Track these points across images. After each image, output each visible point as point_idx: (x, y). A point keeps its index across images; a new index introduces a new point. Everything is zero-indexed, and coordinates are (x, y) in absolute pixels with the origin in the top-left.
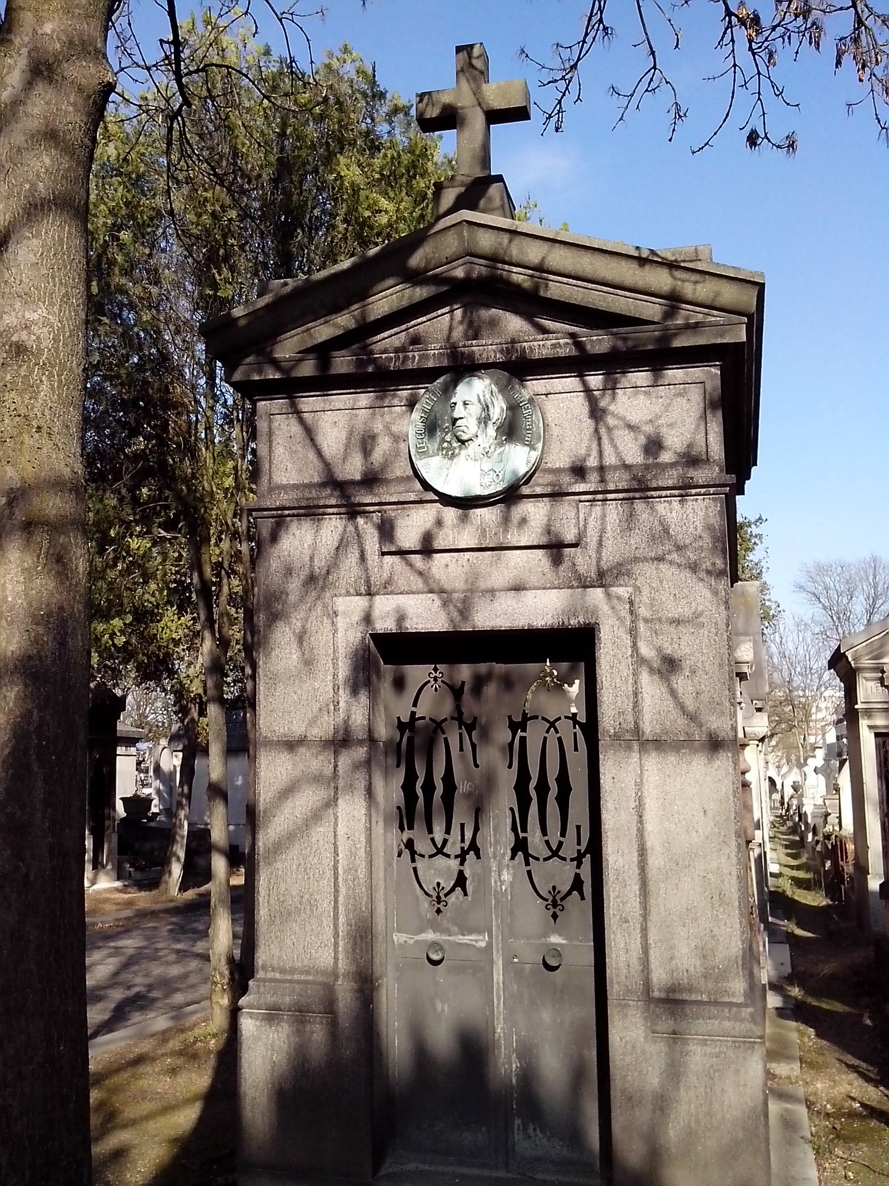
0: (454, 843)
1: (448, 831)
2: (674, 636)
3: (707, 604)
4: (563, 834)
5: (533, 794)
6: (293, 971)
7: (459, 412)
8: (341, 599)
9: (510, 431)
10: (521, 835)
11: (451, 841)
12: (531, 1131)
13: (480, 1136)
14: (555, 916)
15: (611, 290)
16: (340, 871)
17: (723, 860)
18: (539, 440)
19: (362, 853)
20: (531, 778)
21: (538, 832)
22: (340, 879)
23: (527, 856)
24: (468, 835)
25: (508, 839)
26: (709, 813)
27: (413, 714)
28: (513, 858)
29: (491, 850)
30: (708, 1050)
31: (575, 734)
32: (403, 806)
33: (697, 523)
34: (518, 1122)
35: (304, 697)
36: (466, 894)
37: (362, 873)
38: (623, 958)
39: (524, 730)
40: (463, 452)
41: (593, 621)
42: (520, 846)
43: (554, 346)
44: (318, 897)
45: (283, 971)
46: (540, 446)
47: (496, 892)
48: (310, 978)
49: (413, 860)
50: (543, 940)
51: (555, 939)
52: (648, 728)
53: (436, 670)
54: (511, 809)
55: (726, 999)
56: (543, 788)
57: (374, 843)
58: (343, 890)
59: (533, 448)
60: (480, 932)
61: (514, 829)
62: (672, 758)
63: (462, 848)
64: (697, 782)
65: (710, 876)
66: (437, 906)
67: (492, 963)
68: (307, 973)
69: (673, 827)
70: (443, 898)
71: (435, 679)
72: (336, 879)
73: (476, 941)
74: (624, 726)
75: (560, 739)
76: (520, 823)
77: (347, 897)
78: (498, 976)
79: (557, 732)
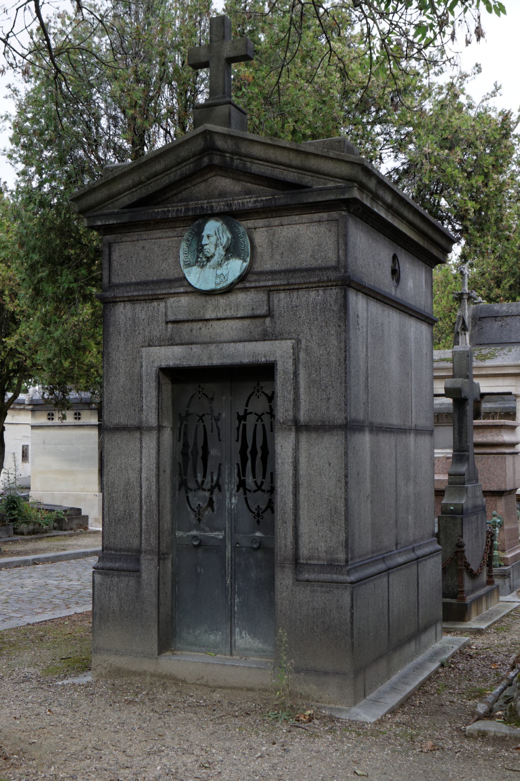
0: (207, 483)
1: (204, 476)
2: (318, 367)
3: (335, 349)
4: (264, 477)
5: (249, 455)
6: (121, 550)
7: (205, 241)
8: (144, 349)
9: (232, 251)
10: (242, 478)
11: (206, 481)
12: (244, 635)
13: (218, 637)
14: (258, 522)
15: (286, 168)
16: (143, 497)
17: (338, 490)
18: (248, 256)
19: (154, 487)
20: (248, 447)
21: (251, 477)
22: (143, 501)
23: (245, 490)
24: (215, 478)
25: (236, 479)
26: (332, 465)
27: (246, 410)
28: (238, 491)
29: (226, 487)
30: (324, 589)
31: (212, 423)
32: (181, 462)
33: (332, 302)
34: (237, 630)
35: (127, 404)
36: (213, 510)
37: (154, 498)
38: (283, 542)
39: (245, 420)
40: (208, 264)
41: (274, 359)
42: (242, 484)
43: (255, 202)
44: (133, 512)
45: (116, 550)
46: (248, 259)
47: (228, 509)
48: (129, 554)
49: (187, 493)
50: (252, 535)
51: (258, 534)
52: (303, 417)
53: (199, 387)
54: (238, 464)
55: (336, 564)
56: (254, 452)
57: (162, 483)
58: (144, 507)
59: (244, 261)
60: (220, 530)
61: (239, 475)
62: (314, 435)
63: (212, 486)
64: (326, 448)
65: (331, 498)
66: (198, 517)
67: (225, 546)
68: (128, 551)
69: (313, 472)
70: (202, 513)
71: (199, 392)
72: (141, 501)
73: (218, 535)
74: (288, 417)
75: (204, 426)
76: (242, 472)
77: (147, 511)
78: (228, 554)
79: (262, 421)
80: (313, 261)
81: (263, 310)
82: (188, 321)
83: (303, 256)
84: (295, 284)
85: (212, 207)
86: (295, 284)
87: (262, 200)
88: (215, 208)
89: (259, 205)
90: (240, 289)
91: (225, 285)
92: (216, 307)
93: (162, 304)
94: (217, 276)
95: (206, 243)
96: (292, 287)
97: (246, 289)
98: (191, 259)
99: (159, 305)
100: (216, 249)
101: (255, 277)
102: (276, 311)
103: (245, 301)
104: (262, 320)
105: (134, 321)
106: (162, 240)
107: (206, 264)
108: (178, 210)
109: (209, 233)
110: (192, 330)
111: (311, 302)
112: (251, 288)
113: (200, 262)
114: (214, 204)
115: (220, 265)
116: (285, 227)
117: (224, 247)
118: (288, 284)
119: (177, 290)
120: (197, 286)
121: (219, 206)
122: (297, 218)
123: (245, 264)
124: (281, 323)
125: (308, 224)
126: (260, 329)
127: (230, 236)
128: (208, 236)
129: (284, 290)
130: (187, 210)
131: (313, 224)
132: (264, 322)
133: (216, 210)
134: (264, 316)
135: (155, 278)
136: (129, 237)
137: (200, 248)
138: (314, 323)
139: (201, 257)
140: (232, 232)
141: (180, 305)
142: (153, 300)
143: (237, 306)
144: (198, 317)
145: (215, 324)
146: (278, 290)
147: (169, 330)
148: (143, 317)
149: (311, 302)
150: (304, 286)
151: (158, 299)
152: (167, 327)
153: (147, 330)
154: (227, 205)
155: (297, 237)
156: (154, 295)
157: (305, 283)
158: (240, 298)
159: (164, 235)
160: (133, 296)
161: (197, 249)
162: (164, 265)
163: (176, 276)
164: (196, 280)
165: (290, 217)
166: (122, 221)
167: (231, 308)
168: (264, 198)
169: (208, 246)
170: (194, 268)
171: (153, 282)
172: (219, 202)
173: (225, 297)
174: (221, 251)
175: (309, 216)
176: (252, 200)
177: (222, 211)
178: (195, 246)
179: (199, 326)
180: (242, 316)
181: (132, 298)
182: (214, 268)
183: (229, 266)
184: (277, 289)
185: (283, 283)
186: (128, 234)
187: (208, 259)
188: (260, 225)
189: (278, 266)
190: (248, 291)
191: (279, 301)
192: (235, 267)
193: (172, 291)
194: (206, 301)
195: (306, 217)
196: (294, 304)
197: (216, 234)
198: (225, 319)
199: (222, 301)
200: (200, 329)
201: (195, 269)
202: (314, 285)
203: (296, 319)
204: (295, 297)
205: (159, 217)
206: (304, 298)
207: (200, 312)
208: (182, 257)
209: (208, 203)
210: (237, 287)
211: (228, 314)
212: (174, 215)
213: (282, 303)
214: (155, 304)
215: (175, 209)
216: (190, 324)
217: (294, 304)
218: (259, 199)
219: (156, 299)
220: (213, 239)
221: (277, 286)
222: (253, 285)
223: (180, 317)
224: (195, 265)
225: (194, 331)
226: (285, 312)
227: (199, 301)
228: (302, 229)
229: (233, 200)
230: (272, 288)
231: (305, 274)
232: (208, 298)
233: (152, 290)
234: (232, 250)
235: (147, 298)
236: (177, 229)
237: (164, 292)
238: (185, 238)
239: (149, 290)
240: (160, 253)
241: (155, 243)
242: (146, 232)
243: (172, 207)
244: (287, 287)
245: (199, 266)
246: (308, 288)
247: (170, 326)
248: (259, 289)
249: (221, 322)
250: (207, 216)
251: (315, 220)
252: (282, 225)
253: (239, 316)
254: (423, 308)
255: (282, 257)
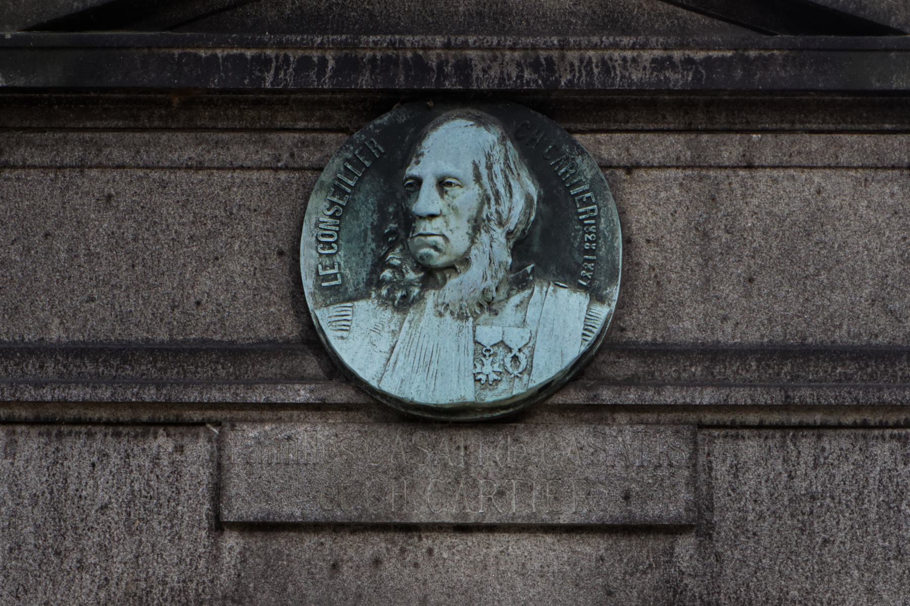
7: (427, 200)
9: (545, 251)
40: (431, 297)
43: (659, 64)
46: (615, 292)
59: (597, 297)
80: (883, 321)
81: (672, 505)
82: (316, 527)
83: (837, 297)
84: (811, 408)
85: (464, 67)
86: (811, 408)
87: (689, 61)
88: (477, 72)
89: (677, 79)
90: (565, 410)
91: (518, 389)
92: (461, 480)
93: (199, 448)
94: (481, 352)
95: (433, 210)
96: (795, 419)
97: (596, 413)
98: (349, 266)
99: (180, 449)
100: (473, 242)
101: (630, 366)
102: (724, 509)
103: (584, 462)
104: (660, 543)
105: (55, 507)
106: (201, 175)
107: (421, 298)
108: (305, 63)
109: (448, 168)
110: (335, 567)
111: (873, 485)
112: (615, 408)
113: (393, 285)
114: (471, 54)
115: (488, 305)
116: (760, 173)
117: (509, 234)
118: (787, 407)
119: (279, 395)
120: (390, 386)
121: (496, 64)
122: (816, 143)
123: (602, 312)
124: (744, 562)
125: (860, 174)
126: (650, 579)
127: (533, 190)
128: (443, 184)
129: (761, 426)
130: (349, 65)
131: (882, 174)
132: (670, 552)
133: (485, 78)
134: (674, 529)
135: (162, 335)
136: (43, 146)
137: (397, 224)
138: (886, 570)
139: (398, 262)
140: (541, 174)
141: (292, 457)
142: (152, 425)
143: (557, 478)
144: (374, 512)
145: (446, 546)
146: (733, 426)
147: (227, 559)
148: (103, 496)
149: (873, 485)
150: (849, 419)
151: (178, 423)
152: (215, 544)
153: (123, 553)
154: (535, 66)
155: (813, 218)
156: (168, 405)
157: (858, 408)
158: (568, 444)
159: (212, 156)
160: (64, 404)
161: (377, 229)
162: (205, 282)
163: (263, 332)
164: (379, 360)
165: (786, 138)
166: (36, 81)
167: (526, 487)
168: (700, 55)
169: (438, 223)
170: (362, 305)
171: (154, 351)
172: (500, 47)
173: (502, 439)
174: (496, 247)
175: (869, 141)
176: (647, 55)
177: (509, 85)
178: (367, 216)
179: (368, 553)
180: (578, 520)
181: (50, 412)
182: (462, 317)
183: (532, 312)
184: (731, 423)
185: (763, 398)
186: (37, 137)
187: (432, 276)
188: (657, 158)
189: (728, 327)
190: (602, 421)
191: (736, 470)
192: (558, 324)
193: (258, 396)
194: (415, 450)
195: (855, 145)
196: (801, 485)
197: (478, 178)
198: (491, 528)
199: (488, 453)
200: (377, 562)
201: (366, 312)
202: (892, 419)
203: (810, 550)
204: (807, 456)
205: (214, 83)
206: (847, 467)
207: (382, 491)
208: (308, 258)
209: (447, 46)
210: (559, 399)
211: (514, 508)
212: (288, 78)
213: (750, 481)
214: (163, 443)
215: (294, 55)
216: (327, 540)
217: (801, 485)
218: (677, 55)
219: (166, 424)
220: (466, 197)
221: (736, 408)
222: (631, 396)
223: (291, 509)
224: (366, 296)
225: (346, 570)
226: (761, 517)
227: (391, 443)
228: (838, 187)
229: (563, 46)
230: (708, 418)
231: (851, 368)
232: (419, 437)
233: (159, 386)
234: (536, 248)
235: (125, 415)
236: (274, 137)
237: (216, 396)
238: (326, 177)
239: (144, 384)
240: (186, 232)
241: (163, 185)
242: (128, 137)
243: (280, 45)
244: (775, 418)
245: (386, 301)
246: (865, 425)
247: (232, 541)
248: (651, 417)
249: (472, 540)
250: (434, 99)
251: (893, 157)
252: (750, 167)
253: (564, 519)
254: (277, 535)
255: (748, 295)
